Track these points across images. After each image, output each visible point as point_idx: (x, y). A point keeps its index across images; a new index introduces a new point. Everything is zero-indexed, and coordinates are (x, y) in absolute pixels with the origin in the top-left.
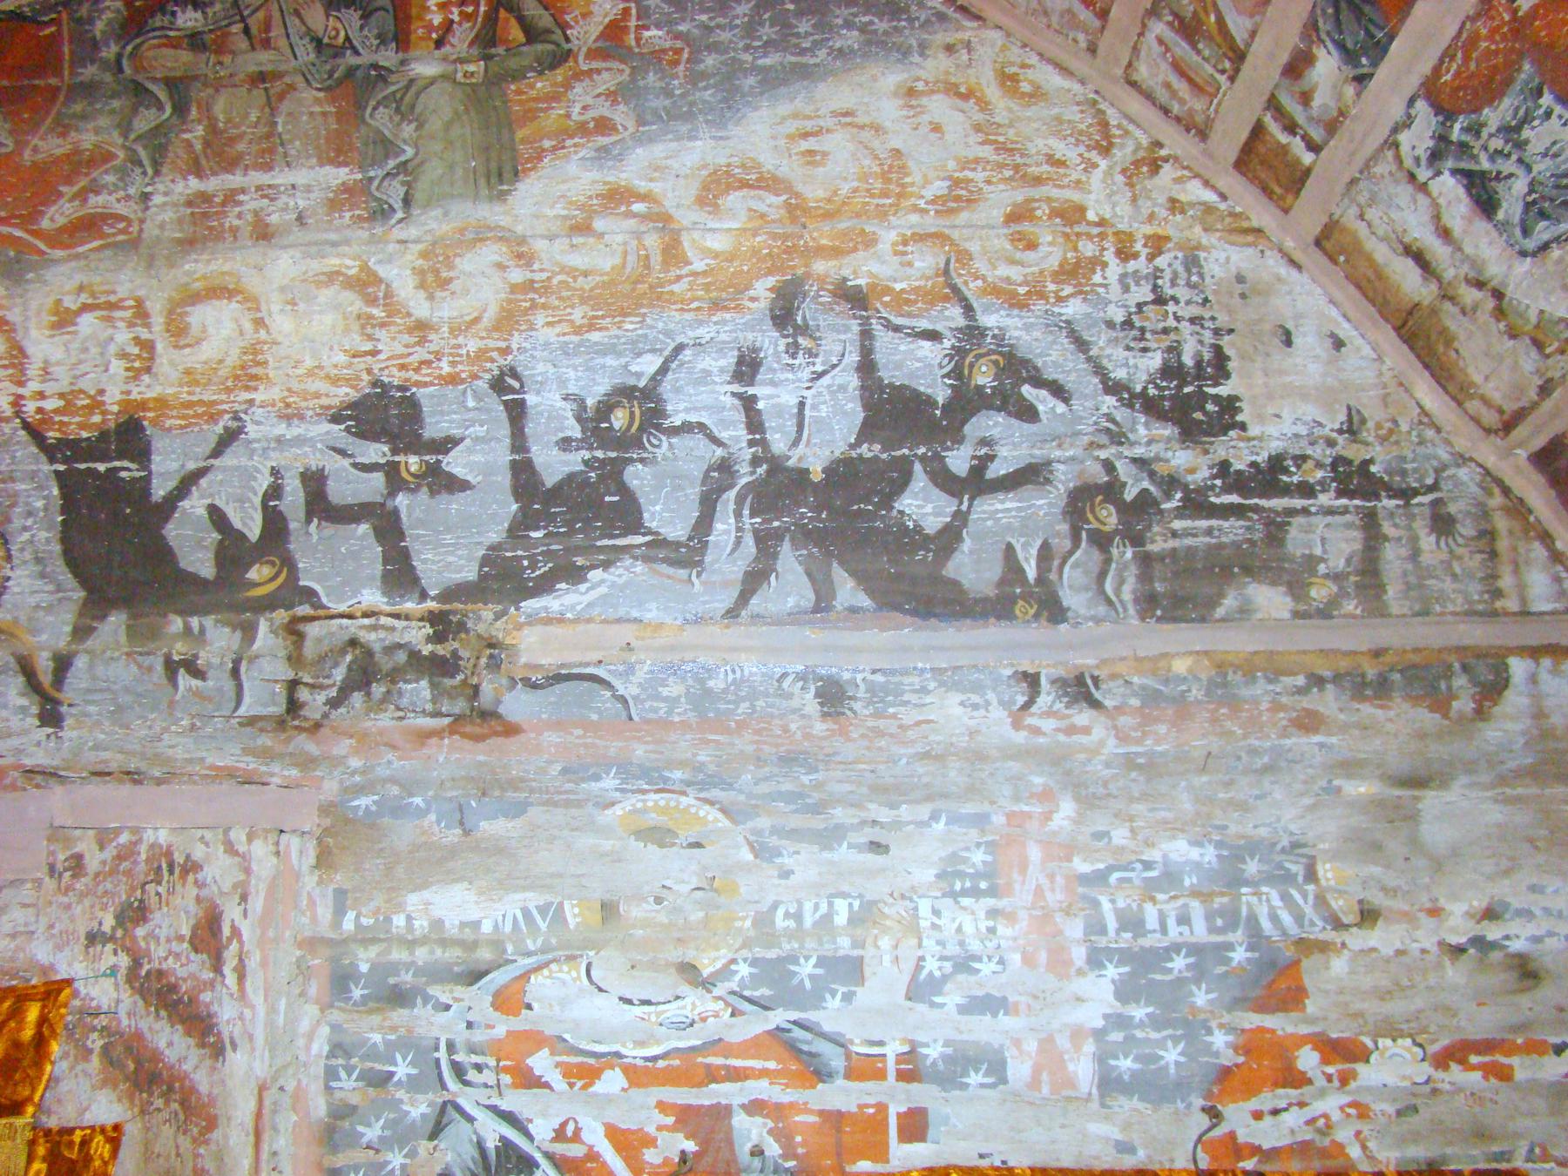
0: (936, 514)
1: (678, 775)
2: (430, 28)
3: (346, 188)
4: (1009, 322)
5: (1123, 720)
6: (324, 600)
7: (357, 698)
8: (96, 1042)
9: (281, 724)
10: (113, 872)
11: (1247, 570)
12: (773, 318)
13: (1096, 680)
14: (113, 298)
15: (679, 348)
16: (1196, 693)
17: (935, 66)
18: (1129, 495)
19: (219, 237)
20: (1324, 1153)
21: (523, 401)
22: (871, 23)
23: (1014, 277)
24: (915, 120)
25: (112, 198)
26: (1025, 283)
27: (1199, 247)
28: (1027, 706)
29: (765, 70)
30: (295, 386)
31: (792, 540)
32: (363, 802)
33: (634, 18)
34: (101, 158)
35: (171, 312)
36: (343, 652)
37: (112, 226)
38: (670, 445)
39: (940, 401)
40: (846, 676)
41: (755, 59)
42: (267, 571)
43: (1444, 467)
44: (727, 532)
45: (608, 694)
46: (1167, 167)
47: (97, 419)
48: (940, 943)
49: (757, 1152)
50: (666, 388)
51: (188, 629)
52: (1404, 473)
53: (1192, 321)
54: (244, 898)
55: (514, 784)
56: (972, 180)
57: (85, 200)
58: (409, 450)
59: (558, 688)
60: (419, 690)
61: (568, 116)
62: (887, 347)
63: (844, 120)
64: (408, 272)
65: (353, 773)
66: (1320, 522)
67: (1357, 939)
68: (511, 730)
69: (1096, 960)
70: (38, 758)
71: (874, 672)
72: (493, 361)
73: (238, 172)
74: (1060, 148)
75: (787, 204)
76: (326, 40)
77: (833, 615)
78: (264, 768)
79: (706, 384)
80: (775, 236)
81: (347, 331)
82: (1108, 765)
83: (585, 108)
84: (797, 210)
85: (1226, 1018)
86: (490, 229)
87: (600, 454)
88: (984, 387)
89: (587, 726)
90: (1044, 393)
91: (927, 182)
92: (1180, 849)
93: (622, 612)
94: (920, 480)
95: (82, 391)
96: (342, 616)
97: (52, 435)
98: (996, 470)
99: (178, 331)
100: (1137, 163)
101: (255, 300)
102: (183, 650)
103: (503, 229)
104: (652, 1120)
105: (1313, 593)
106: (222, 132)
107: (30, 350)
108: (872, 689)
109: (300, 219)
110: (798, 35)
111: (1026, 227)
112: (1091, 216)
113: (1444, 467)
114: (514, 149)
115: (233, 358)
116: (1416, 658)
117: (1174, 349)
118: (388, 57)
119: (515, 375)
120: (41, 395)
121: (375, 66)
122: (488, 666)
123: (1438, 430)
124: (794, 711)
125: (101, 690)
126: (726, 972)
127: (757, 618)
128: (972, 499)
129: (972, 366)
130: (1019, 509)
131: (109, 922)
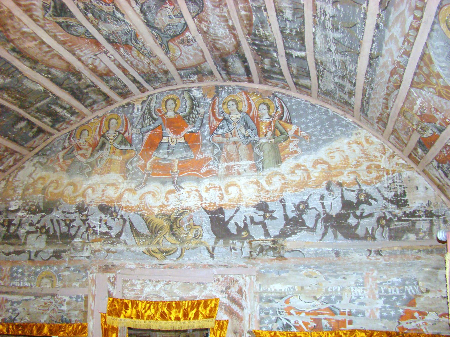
1: (312, 266)
2: (263, 133)
3: (252, 165)
4: (367, 188)
5: (386, 258)
7: (261, 254)
8: (223, 307)
9: (249, 258)
10: (224, 281)
11: (408, 231)
13: (381, 251)
15: (311, 195)
16: (398, 253)
17: (354, 138)
18: (388, 218)
19: (232, 174)
20: (418, 330)
27: (401, 172)
28: (369, 255)
29: (323, 140)
32: (263, 270)
34: (209, 159)
35: (225, 188)
40: (339, 250)
42: (245, 233)
43: (446, 211)
46: (396, 156)
47: (215, 207)
48: (355, 294)
49: (326, 326)
50: (309, 201)
51: (233, 242)
52: (438, 212)
53: (400, 186)
54: (246, 286)
55: (287, 268)
57: (208, 167)
58: (267, 212)
59: (293, 252)
60: (271, 253)
61: (289, 150)
66: (422, 222)
67: (425, 295)
68: (286, 259)
69: (380, 297)
70: (211, 263)
73: (233, 161)
74: (377, 154)
75: (328, 167)
80: (326, 173)
81: (255, 192)
82: (383, 265)
84: (330, 168)
85: (402, 307)
89: (298, 258)
90: (373, 200)
91: (352, 162)
92: (395, 279)
94: (352, 216)
98: (365, 214)
99: (227, 192)
100: (390, 156)
104: (309, 321)
105: (420, 235)
108: (344, 253)
109: (245, 171)
110: (329, 132)
111: (370, 169)
112: (382, 167)
113: (446, 211)
114: (280, 157)
115: (237, 197)
116: (438, 247)
117: (396, 192)
118: (257, 138)
119: (284, 200)
120: (205, 203)
121: (255, 140)
123: (445, 204)
126: (321, 298)
131: (224, 289)
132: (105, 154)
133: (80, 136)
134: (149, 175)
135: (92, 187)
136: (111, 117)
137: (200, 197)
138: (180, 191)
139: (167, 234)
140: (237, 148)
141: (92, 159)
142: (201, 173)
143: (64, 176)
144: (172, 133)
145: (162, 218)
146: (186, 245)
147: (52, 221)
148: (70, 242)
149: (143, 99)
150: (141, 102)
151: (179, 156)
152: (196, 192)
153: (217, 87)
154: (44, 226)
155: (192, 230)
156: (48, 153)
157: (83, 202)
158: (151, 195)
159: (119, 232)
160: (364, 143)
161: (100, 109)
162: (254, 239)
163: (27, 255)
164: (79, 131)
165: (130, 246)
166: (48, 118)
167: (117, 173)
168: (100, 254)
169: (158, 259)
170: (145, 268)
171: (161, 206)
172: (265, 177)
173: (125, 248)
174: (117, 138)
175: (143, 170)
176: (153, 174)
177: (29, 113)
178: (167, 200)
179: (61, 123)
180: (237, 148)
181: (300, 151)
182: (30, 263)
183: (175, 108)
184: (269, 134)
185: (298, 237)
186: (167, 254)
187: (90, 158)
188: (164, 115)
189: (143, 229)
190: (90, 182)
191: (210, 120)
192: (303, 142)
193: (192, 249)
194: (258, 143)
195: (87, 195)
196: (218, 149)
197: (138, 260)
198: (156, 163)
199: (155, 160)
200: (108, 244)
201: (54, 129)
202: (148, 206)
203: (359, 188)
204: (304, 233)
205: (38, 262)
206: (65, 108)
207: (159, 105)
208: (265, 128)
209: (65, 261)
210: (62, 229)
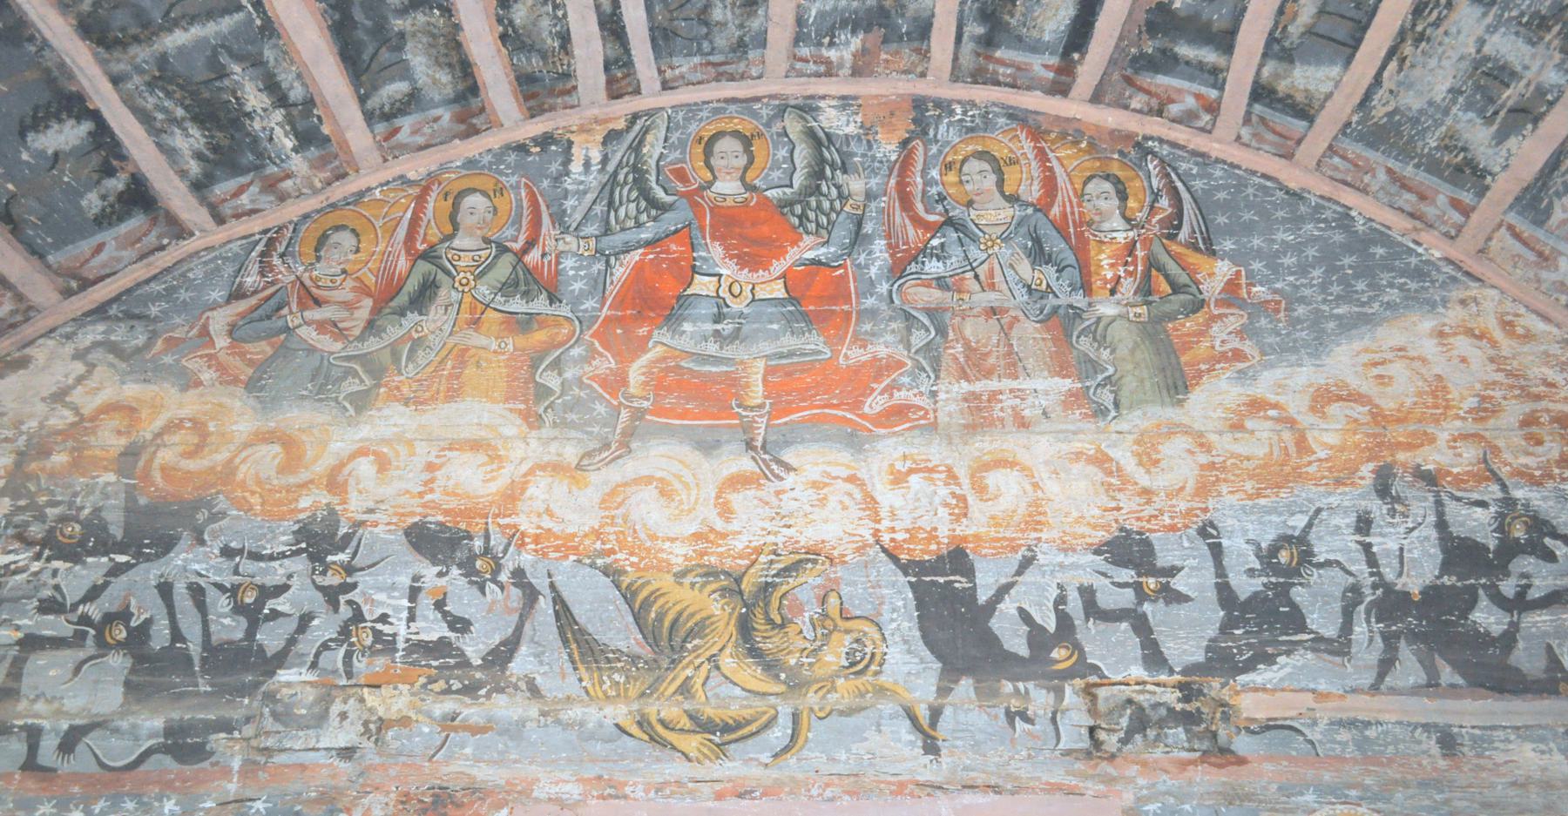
0: (1497, 624)
1: (1353, 793)
2: (1106, 282)
3: (1071, 393)
6: (1106, 673)
7: (1138, 738)
9: (1088, 754)
12: (1377, 491)
14: (930, 465)
15: (1319, 511)
17: (1454, 315)
19: (992, 424)
21: (1220, 544)
22: (1406, 284)
23: (1530, 464)
24: (1448, 354)
25: (910, 393)
26: (1539, 468)
29: (1339, 317)
30: (1068, 530)
31: (1407, 639)
33: (1244, 278)
35: (972, 476)
36: (1124, 709)
37: (914, 413)
38: (1320, 576)
39: (1492, 548)
41: (1332, 309)
44: (1363, 633)
45: (1301, 738)
47: (933, 547)
50: (1312, 537)
51: (1017, 690)
56: (1493, 397)
57: (892, 395)
59: (1268, 734)
60: (1178, 733)
61: (1213, 347)
62: (1453, 510)
63: (1400, 354)
64: (1129, 454)
65: (1141, 789)
68: (1242, 761)
71: (1473, 727)
72: (1198, 516)
73: (995, 378)
76: (1033, 287)
77: (1440, 690)
78: (1081, 784)
79: (1338, 535)
80: (1368, 435)
83: (1223, 342)
84: (1378, 416)
86: (1178, 426)
87: (1273, 580)
88: (1519, 539)
89: (1290, 759)
90: (1559, 543)
91: (1463, 399)
93: (1303, 685)
94: (1484, 601)
95: (920, 528)
96: (1121, 683)
97: (904, 557)
98: (1534, 594)
99: (980, 489)
101: (1030, 469)
102: (1017, 704)
103: (1185, 426)
106: (976, 350)
107: (879, 499)
109: (1045, 413)
110: (1356, 292)
111: (1534, 429)
114: (1181, 370)
115: (1022, 510)
118: (1079, 300)
119: (1215, 528)
120: (893, 530)
121: (1071, 306)
122: (1222, 719)
124: (1424, 752)
125: (963, 731)
127: (1393, 691)
128: (1519, 614)
129: (1509, 524)
130: (1551, 621)
132: (432, 326)
133: (317, 250)
134: (638, 414)
135: (375, 453)
136: (466, 184)
137: (871, 504)
138: (781, 479)
139: (727, 651)
140: (1006, 331)
141: (372, 344)
142: (863, 416)
143: (238, 404)
144: (732, 263)
145: (704, 585)
146: (812, 698)
147: (165, 590)
148: (257, 685)
149: (611, 126)
150: (600, 138)
151: (768, 348)
152: (849, 487)
153: (919, 104)
154: (124, 615)
155: (835, 636)
156: (154, 310)
157: (332, 512)
158: (655, 493)
159: (503, 643)
160: (1498, 334)
161: (421, 148)
162: (1103, 676)
163: (18, 747)
164: (310, 232)
165: (556, 701)
166: (194, 131)
167: (494, 401)
168: (409, 738)
169: (689, 759)
170: (625, 797)
171: (697, 536)
172: (1130, 438)
173: (534, 712)
174: (489, 267)
175: (614, 395)
176: (659, 411)
177: (116, 80)
178: (726, 512)
179: (243, 180)
180: (1006, 331)
181: (1256, 353)
182: (31, 784)
183: (746, 169)
184: (1128, 287)
185: (1282, 673)
186: (727, 737)
187: (361, 338)
188: (702, 188)
189: (619, 633)
190: (364, 432)
191: (890, 223)
192: (1263, 322)
193: (842, 713)
194: (1085, 316)
195: (352, 482)
196: (927, 330)
197: (593, 761)
198: (668, 370)
199: (664, 359)
200: (448, 691)
201: (203, 201)
202: (642, 536)
203: (1500, 495)
204: (1303, 658)
205: (75, 777)
206: (281, 100)
207: (677, 154)
208: (1112, 265)
209: (226, 772)
210: (213, 628)
